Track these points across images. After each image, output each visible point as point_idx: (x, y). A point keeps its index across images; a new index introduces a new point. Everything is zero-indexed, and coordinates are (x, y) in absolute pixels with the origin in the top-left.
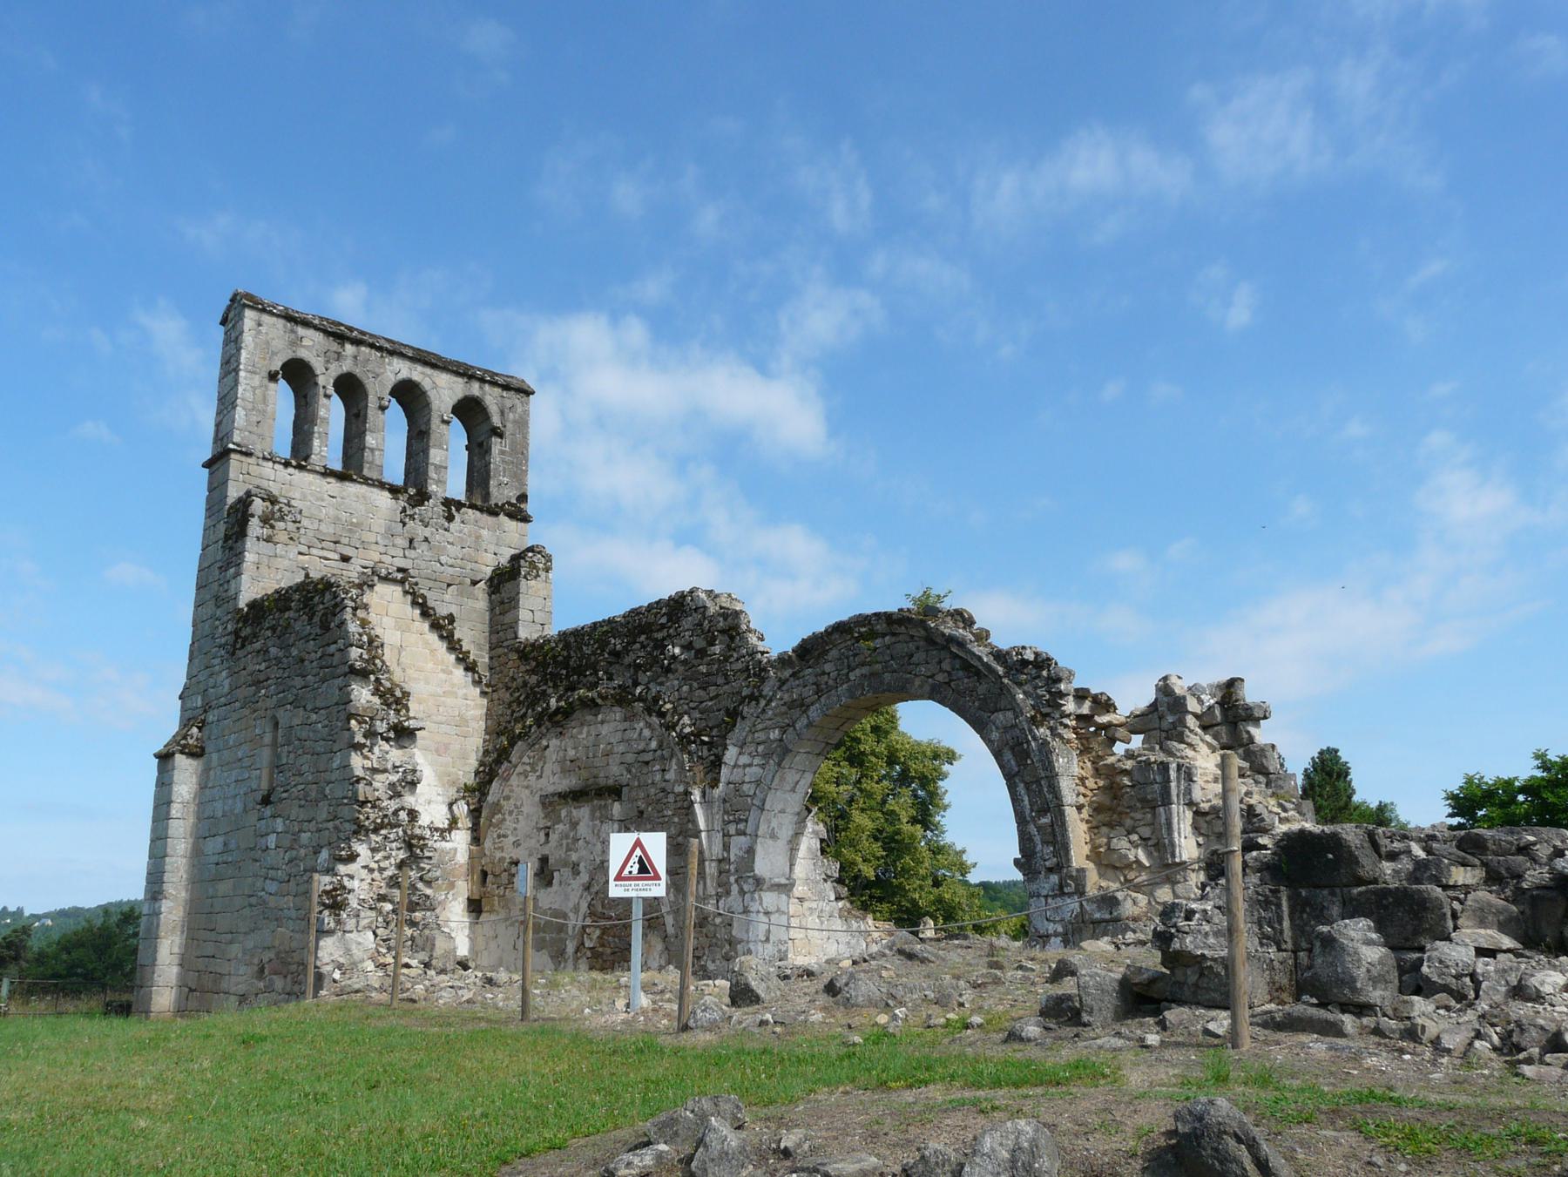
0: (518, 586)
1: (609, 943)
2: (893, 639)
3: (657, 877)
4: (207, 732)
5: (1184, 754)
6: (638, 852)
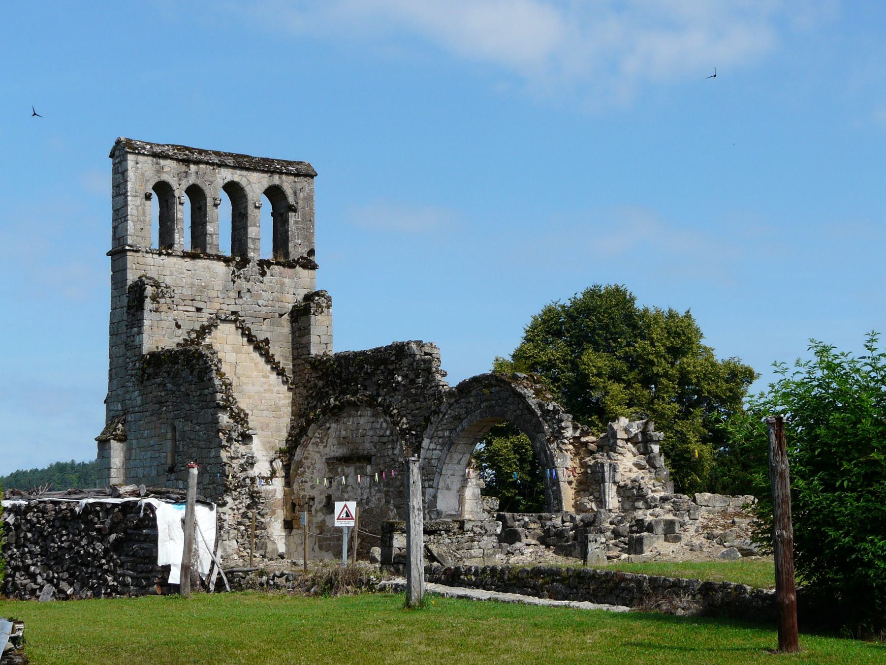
0: (310, 320)
1: (365, 547)
2: (500, 389)
3: (352, 519)
4: (128, 427)
5: (616, 458)
6: (345, 509)
